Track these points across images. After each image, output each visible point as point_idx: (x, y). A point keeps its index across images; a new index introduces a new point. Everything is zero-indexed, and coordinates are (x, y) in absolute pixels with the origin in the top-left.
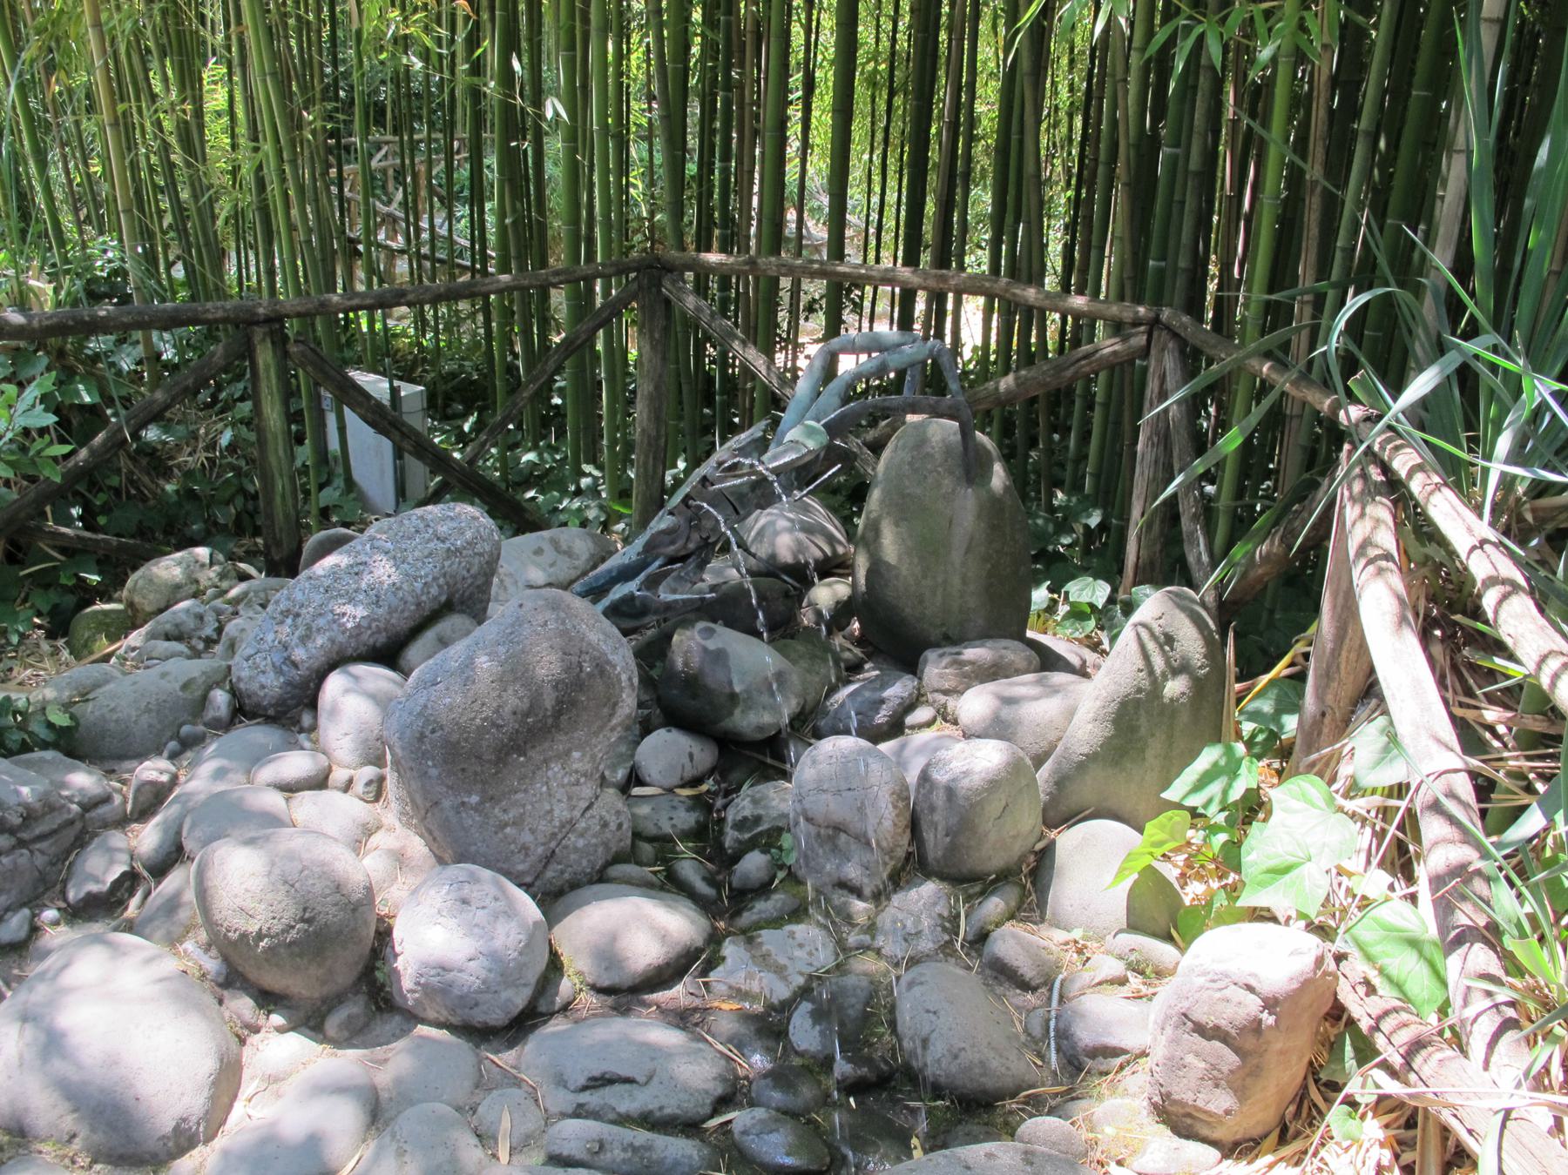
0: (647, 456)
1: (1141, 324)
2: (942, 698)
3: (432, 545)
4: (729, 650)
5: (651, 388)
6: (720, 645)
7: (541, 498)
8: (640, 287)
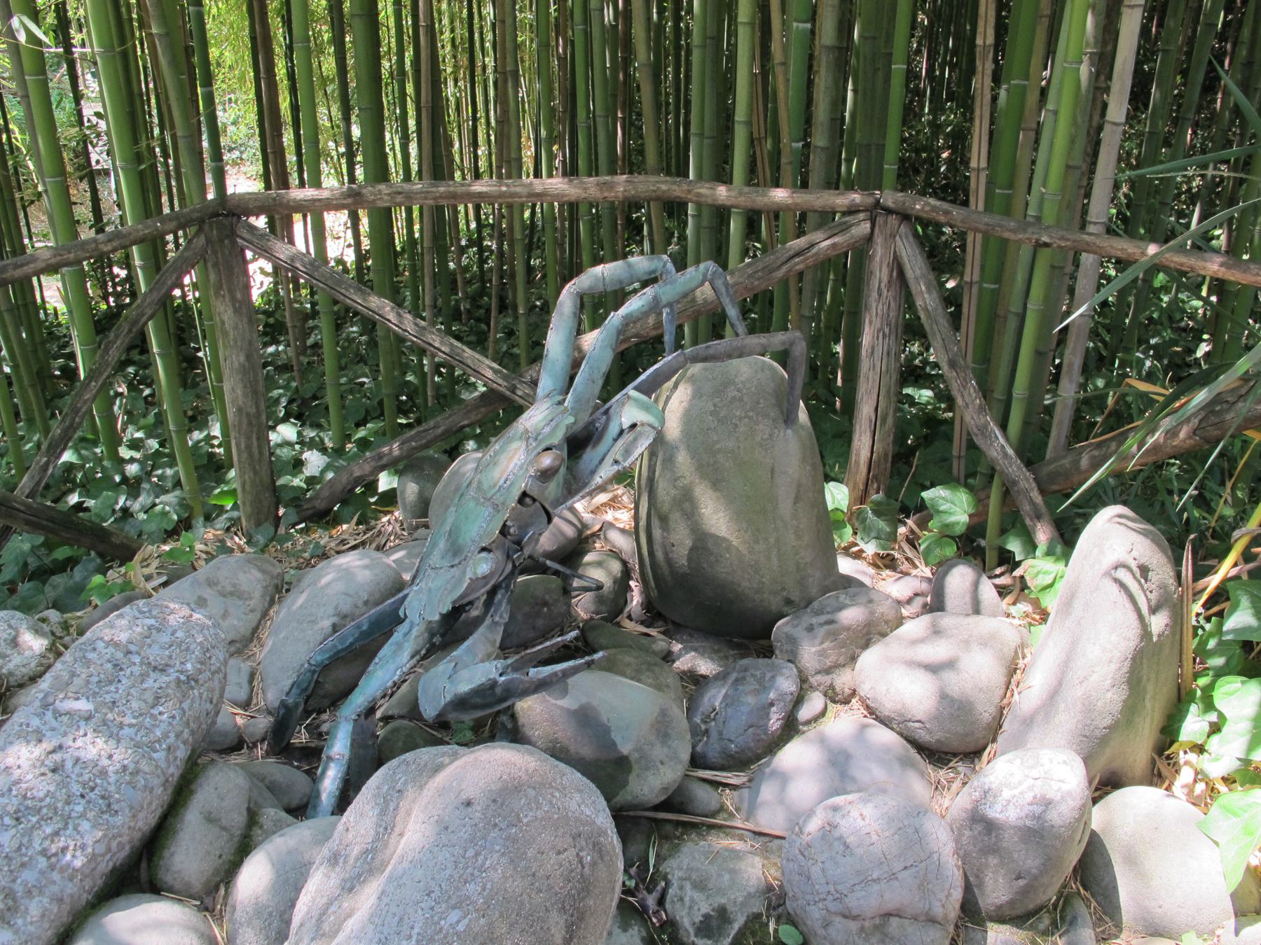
0: (249, 438)
1: (858, 211)
2: (826, 679)
3: (149, 683)
4: (595, 703)
5: (242, 358)
6: (584, 700)
7: (90, 503)
8: (208, 241)
